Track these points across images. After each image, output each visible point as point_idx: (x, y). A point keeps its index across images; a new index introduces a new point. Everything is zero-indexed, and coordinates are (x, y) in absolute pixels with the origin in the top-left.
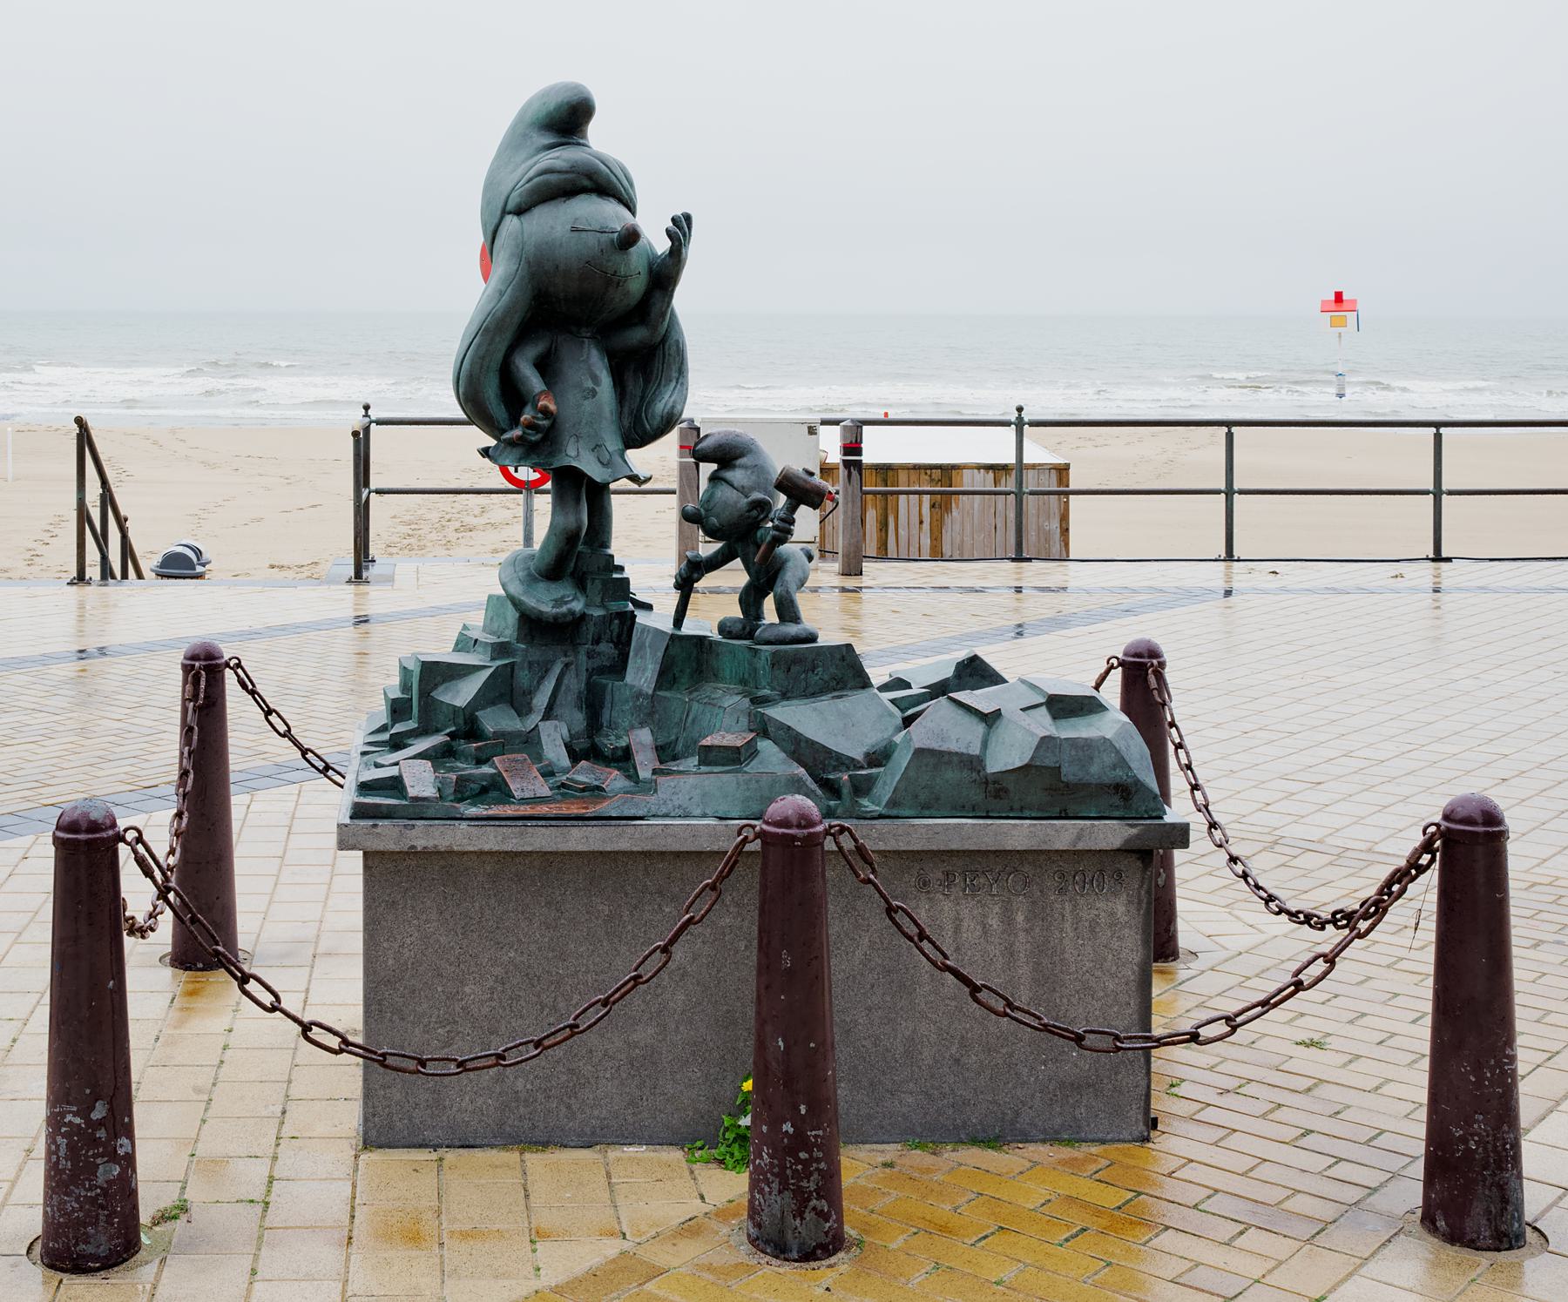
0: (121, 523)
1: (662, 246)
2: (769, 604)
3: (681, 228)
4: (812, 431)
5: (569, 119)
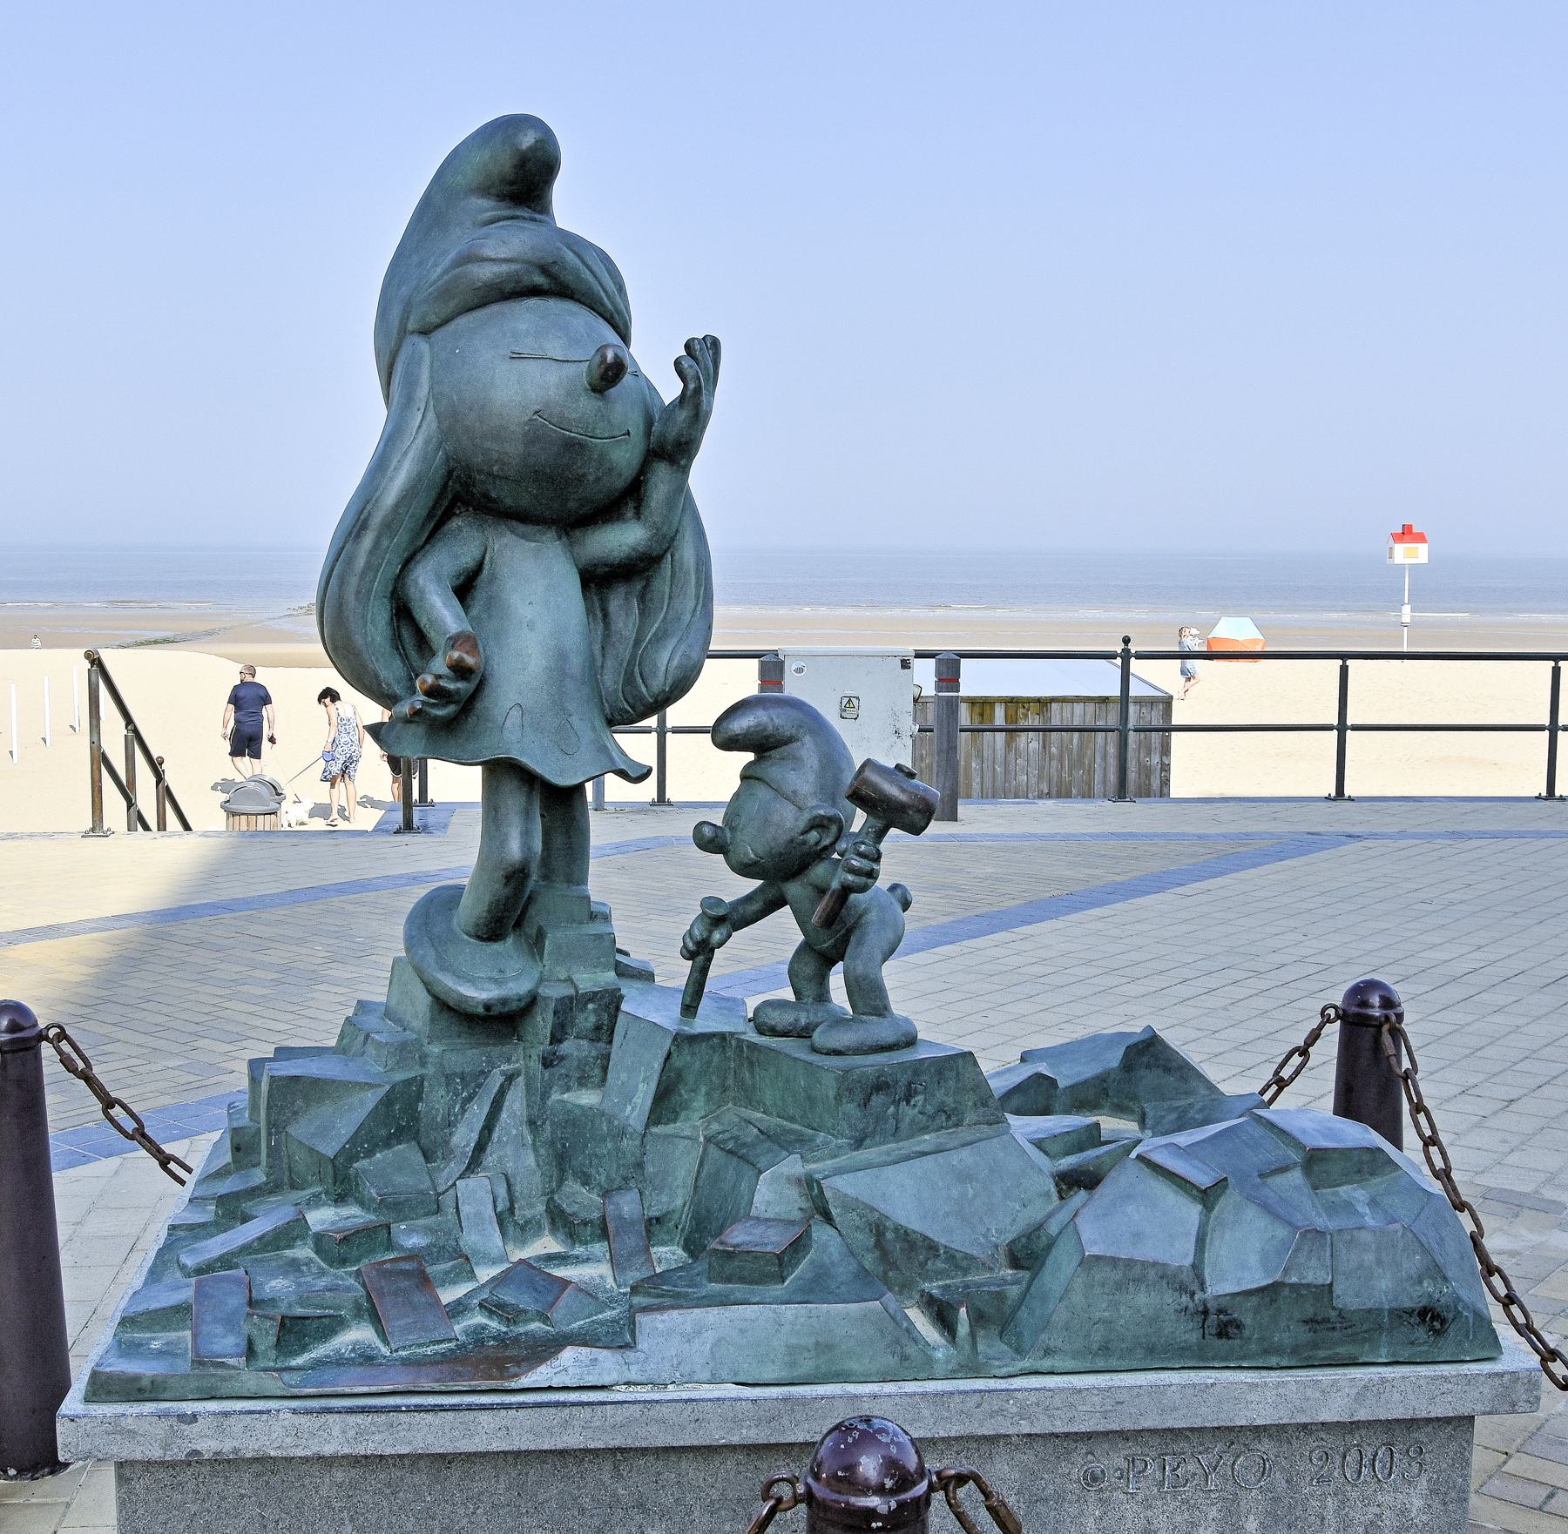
0: (156, 766)
1: (669, 389)
2: (836, 980)
3: (700, 360)
4: (905, 664)
5: (520, 173)
